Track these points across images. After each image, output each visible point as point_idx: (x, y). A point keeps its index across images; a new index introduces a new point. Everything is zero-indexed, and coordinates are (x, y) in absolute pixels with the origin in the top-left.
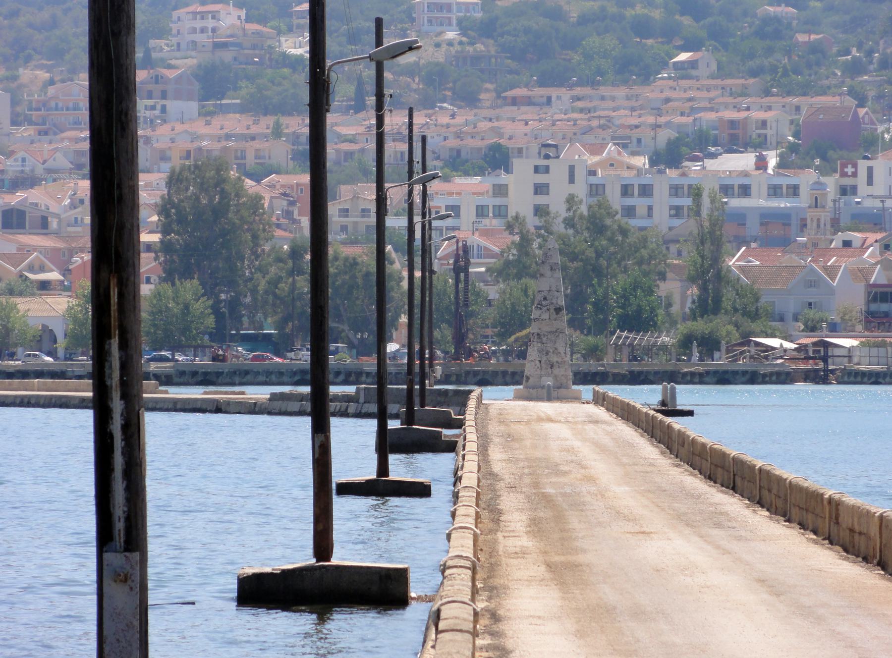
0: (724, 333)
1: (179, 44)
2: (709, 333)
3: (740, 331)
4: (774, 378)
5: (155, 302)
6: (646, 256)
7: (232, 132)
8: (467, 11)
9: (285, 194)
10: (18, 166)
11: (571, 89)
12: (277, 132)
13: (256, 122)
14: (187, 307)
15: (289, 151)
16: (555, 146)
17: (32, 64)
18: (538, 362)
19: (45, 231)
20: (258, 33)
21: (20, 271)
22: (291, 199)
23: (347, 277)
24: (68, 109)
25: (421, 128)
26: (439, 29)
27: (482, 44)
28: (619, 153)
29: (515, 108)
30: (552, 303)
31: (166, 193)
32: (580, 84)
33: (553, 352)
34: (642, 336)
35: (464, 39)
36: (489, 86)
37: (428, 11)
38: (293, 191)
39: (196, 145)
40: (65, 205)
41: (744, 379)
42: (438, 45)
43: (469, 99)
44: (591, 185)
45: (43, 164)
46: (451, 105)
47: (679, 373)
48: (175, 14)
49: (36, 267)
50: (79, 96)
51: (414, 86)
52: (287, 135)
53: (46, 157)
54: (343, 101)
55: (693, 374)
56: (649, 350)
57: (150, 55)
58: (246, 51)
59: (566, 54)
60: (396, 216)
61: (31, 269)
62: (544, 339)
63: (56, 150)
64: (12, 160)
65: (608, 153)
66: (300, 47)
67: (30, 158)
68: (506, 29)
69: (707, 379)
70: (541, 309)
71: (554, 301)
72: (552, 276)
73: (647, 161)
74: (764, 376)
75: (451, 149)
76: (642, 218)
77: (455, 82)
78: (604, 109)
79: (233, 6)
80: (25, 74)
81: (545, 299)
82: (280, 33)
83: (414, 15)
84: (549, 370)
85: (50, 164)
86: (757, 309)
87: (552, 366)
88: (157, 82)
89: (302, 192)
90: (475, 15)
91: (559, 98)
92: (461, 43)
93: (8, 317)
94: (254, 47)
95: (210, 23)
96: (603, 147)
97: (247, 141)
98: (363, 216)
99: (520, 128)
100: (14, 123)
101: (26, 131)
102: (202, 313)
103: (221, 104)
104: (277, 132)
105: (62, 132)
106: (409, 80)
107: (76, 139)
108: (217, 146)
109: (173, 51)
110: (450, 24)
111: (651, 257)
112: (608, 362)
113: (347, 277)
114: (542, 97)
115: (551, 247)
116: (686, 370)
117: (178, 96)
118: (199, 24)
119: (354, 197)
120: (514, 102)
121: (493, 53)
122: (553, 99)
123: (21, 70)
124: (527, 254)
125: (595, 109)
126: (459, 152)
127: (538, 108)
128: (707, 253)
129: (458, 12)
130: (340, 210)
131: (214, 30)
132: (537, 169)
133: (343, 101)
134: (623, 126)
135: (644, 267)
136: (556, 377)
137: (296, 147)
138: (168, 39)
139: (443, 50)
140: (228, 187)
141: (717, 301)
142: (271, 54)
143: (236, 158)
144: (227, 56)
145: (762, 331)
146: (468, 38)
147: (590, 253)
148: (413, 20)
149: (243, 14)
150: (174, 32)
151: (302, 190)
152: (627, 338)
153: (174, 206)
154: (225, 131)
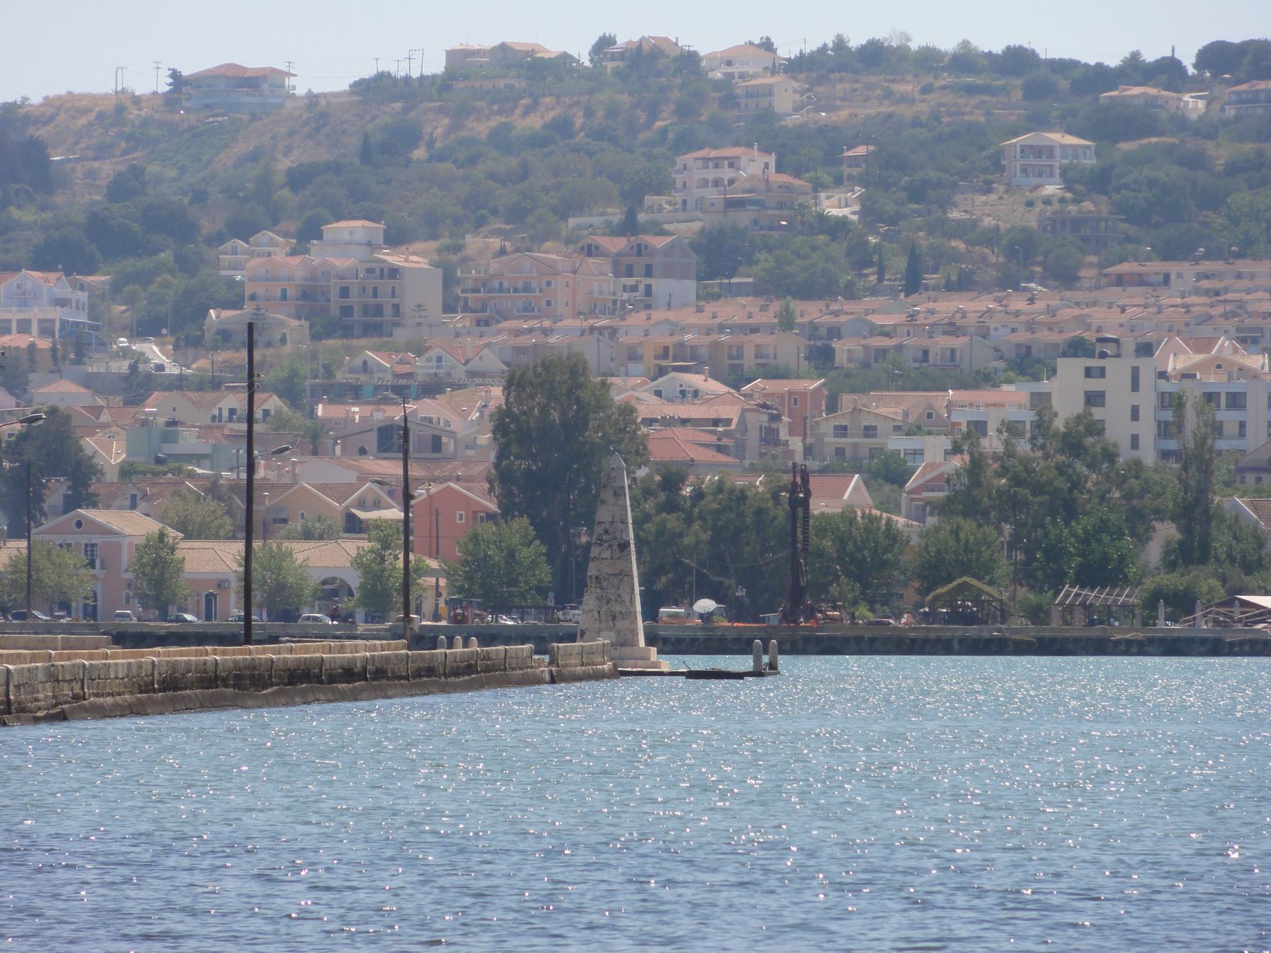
0: (1205, 589)
1: (685, 202)
2: (1185, 589)
3: (1227, 586)
4: (1247, 648)
5: (471, 547)
6: (1137, 489)
7: (729, 322)
8: (1075, 156)
9: (764, 406)
10: (432, 368)
11: (1197, 264)
12: (787, 322)
13: (764, 309)
14: (511, 553)
15: (802, 348)
16: (1116, 341)
17: (484, 229)
18: (595, 613)
19: (436, 455)
20: (787, 187)
21: (347, 508)
22: (775, 412)
23: (733, 516)
24: (516, 290)
25: (981, 317)
26: (1035, 181)
27: (1093, 201)
28: (1236, 351)
29: (1120, 289)
30: (615, 538)
31: (503, 402)
32: (1208, 256)
33: (616, 601)
34: (1098, 593)
35: (1069, 195)
36: (1093, 259)
37: (1022, 157)
38: (782, 404)
39: (677, 339)
40: (472, 420)
41: (1203, 649)
42: (1030, 204)
43: (1064, 277)
44: (1163, 393)
45: (465, 364)
46: (1041, 285)
47: (1110, 641)
48: (680, 161)
49: (369, 502)
50: (532, 272)
51: (992, 259)
52: (802, 326)
53: (469, 355)
54: (895, 280)
55: (1129, 643)
56: (1108, 613)
57: (635, 217)
58: (770, 212)
59: (1207, 216)
60: (907, 435)
61: (362, 505)
62: (605, 584)
63: (488, 345)
64: (424, 358)
65: (1219, 351)
66: (847, 206)
67: (449, 356)
68: (1124, 181)
69: (1150, 649)
70: (601, 545)
71: (618, 536)
72: (615, 504)
73: (1267, 361)
74: (1232, 644)
75: (1018, 346)
76: (1231, 438)
77: (1046, 254)
78: (1237, 291)
79: (759, 150)
80: (473, 243)
81: (606, 532)
82: (818, 186)
83: (1003, 163)
84: (611, 624)
85: (475, 365)
86: (1260, 558)
87: (614, 618)
88: (639, 254)
89: (796, 404)
90: (1085, 162)
91: (1180, 275)
92: (1062, 200)
93: (280, 568)
94: (781, 206)
95: (726, 174)
96: (1211, 342)
97: (746, 334)
98: (867, 436)
99: (1115, 317)
100: (449, 308)
101: (460, 320)
102: (533, 562)
103: (730, 284)
104: (787, 322)
105: (506, 319)
106: (987, 251)
107: (516, 330)
108: (705, 340)
109: (676, 210)
110: (1051, 175)
111: (1144, 491)
112: (1055, 627)
113: (733, 516)
114: (1158, 274)
115: (614, 466)
116: (1119, 637)
117: (668, 273)
118: (711, 174)
119: (855, 409)
120: (1120, 281)
121: (1104, 214)
122: (1173, 277)
123: (468, 237)
124: (978, 484)
125: (1226, 290)
126: (1029, 348)
127: (1149, 290)
128: (1192, 483)
129: (1063, 158)
130: (836, 428)
131: (731, 182)
132: (1088, 372)
133: (895, 280)
134: (1256, 314)
135: (1135, 502)
136: (618, 632)
137: (812, 342)
138: (670, 195)
139: (1037, 210)
140: (585, 395)
141: (1205, 547)
142: (803, 215)
143: (730, 357)
144: (743, 218)
145: (1260, 588)
146: (1073, 193)
147: (1061, 483)
148: (1002, 169)
149: (772, 160)
150: (679, 185)
151: (796, 400)
152: (1077, 595)
153: (515, 419)
154: (717, 321)
